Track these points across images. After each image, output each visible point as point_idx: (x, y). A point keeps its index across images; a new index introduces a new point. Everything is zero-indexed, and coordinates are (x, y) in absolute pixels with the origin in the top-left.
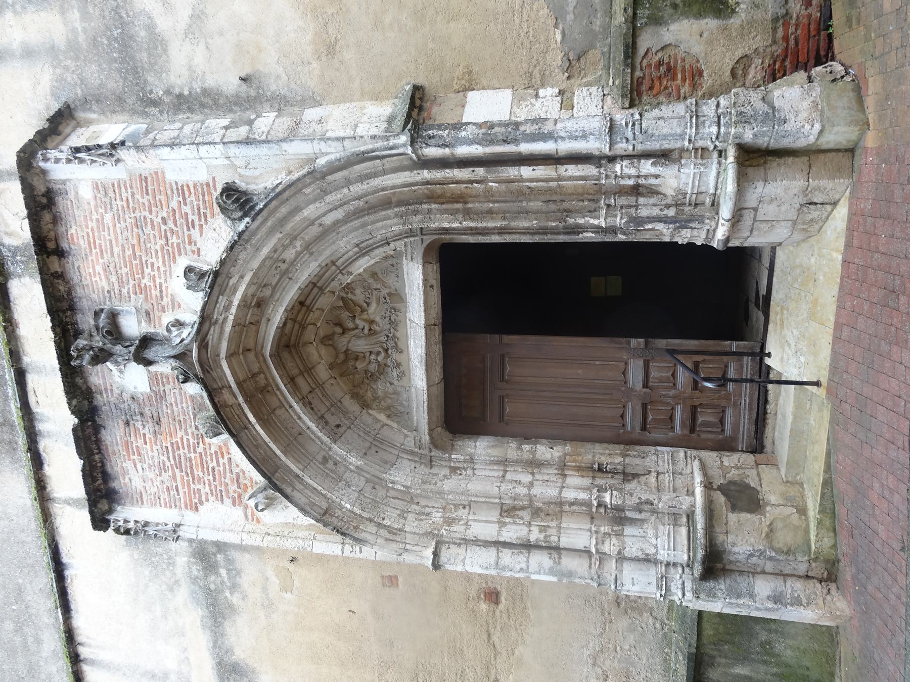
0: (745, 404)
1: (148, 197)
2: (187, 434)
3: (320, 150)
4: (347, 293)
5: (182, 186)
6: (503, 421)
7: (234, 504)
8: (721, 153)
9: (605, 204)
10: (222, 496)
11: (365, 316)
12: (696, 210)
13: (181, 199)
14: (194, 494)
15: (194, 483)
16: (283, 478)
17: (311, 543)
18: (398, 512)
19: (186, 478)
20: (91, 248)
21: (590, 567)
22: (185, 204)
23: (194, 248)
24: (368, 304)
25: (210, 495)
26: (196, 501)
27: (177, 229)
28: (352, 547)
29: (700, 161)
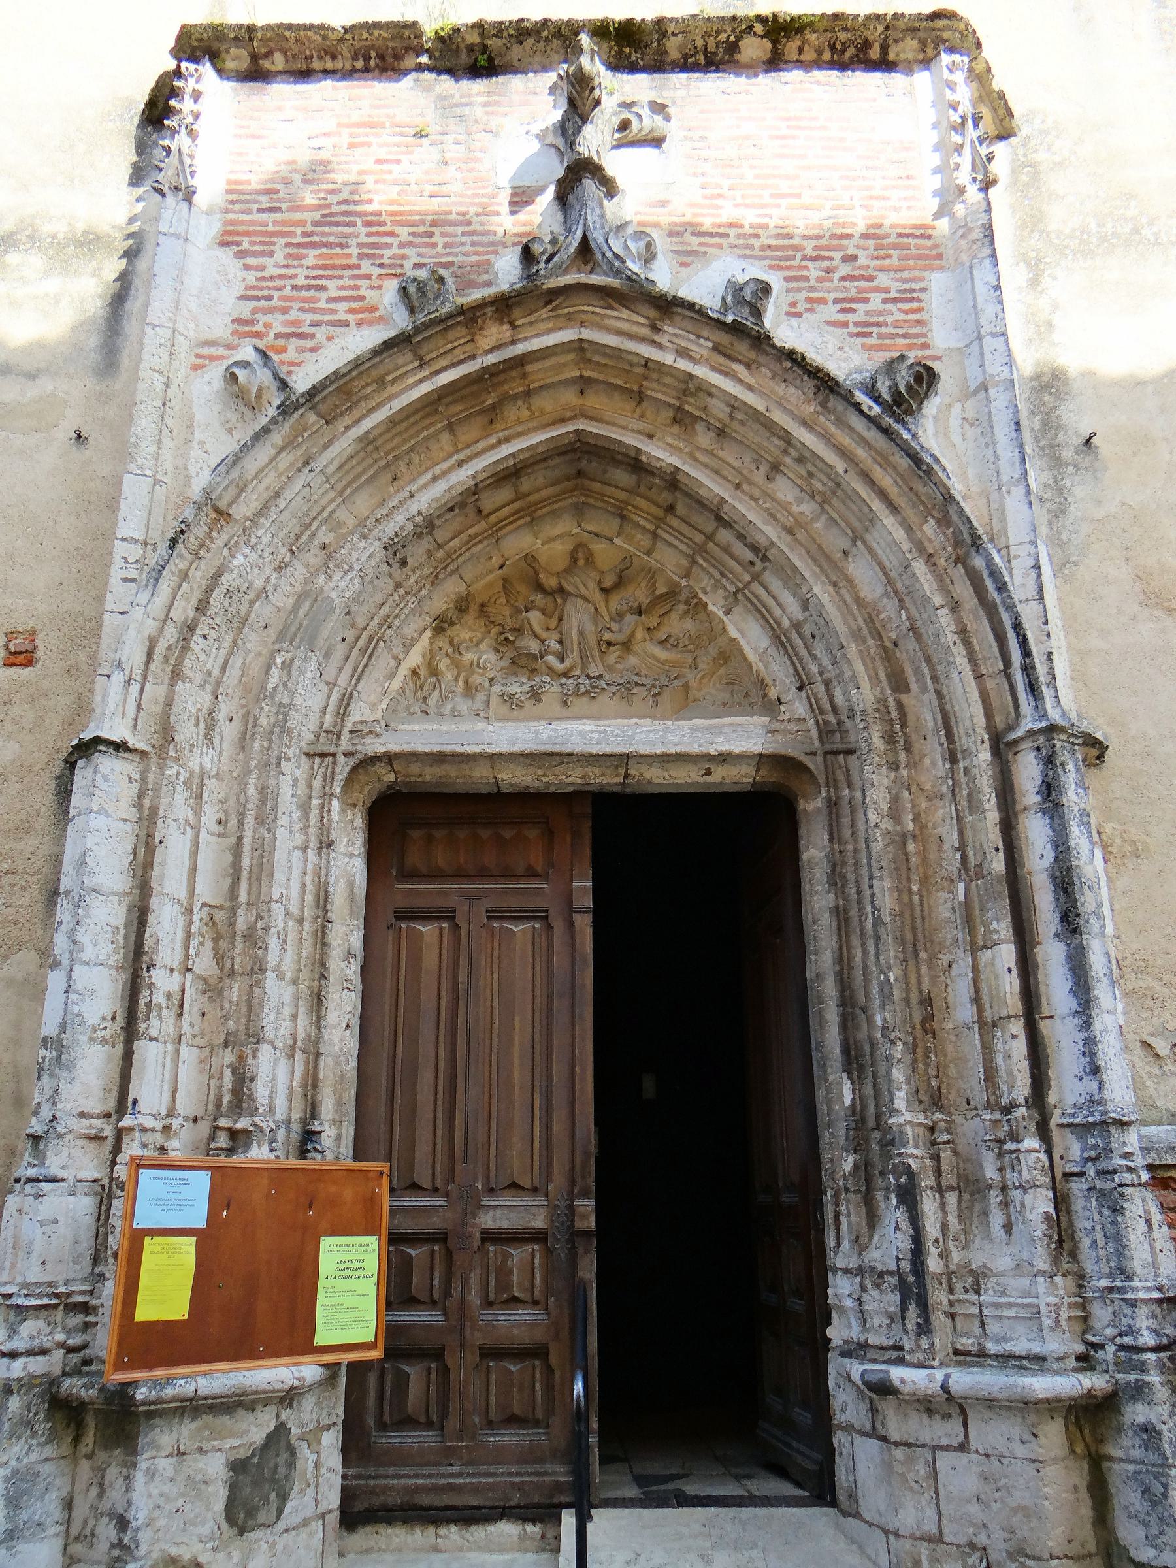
0: (452, 1475)
1: (893, 236)
2: (403, 245)
4: (687, 603)
5: (919, 300)
6: (397, 918)
7: (237, 321)
8: (1085, 1362)
9: (935, 1123)
10: (258, 298)
11: (640, 635)
12: (942, 1317)
13: (893, 295)
14: (262, 243)
15: (287, 245)
16: (305, 430)
17: (148, 472)
18: (216, 672)
19: (299, 231)
20: (789, 119)
21: (82, 1115)
22: (885, 301)
23: (800, 307)
24: (662, 643)
25: (259, 274)
26: (246, 245)
27: (836, 281)
28: (137, 561)
29: (1064, 1315)
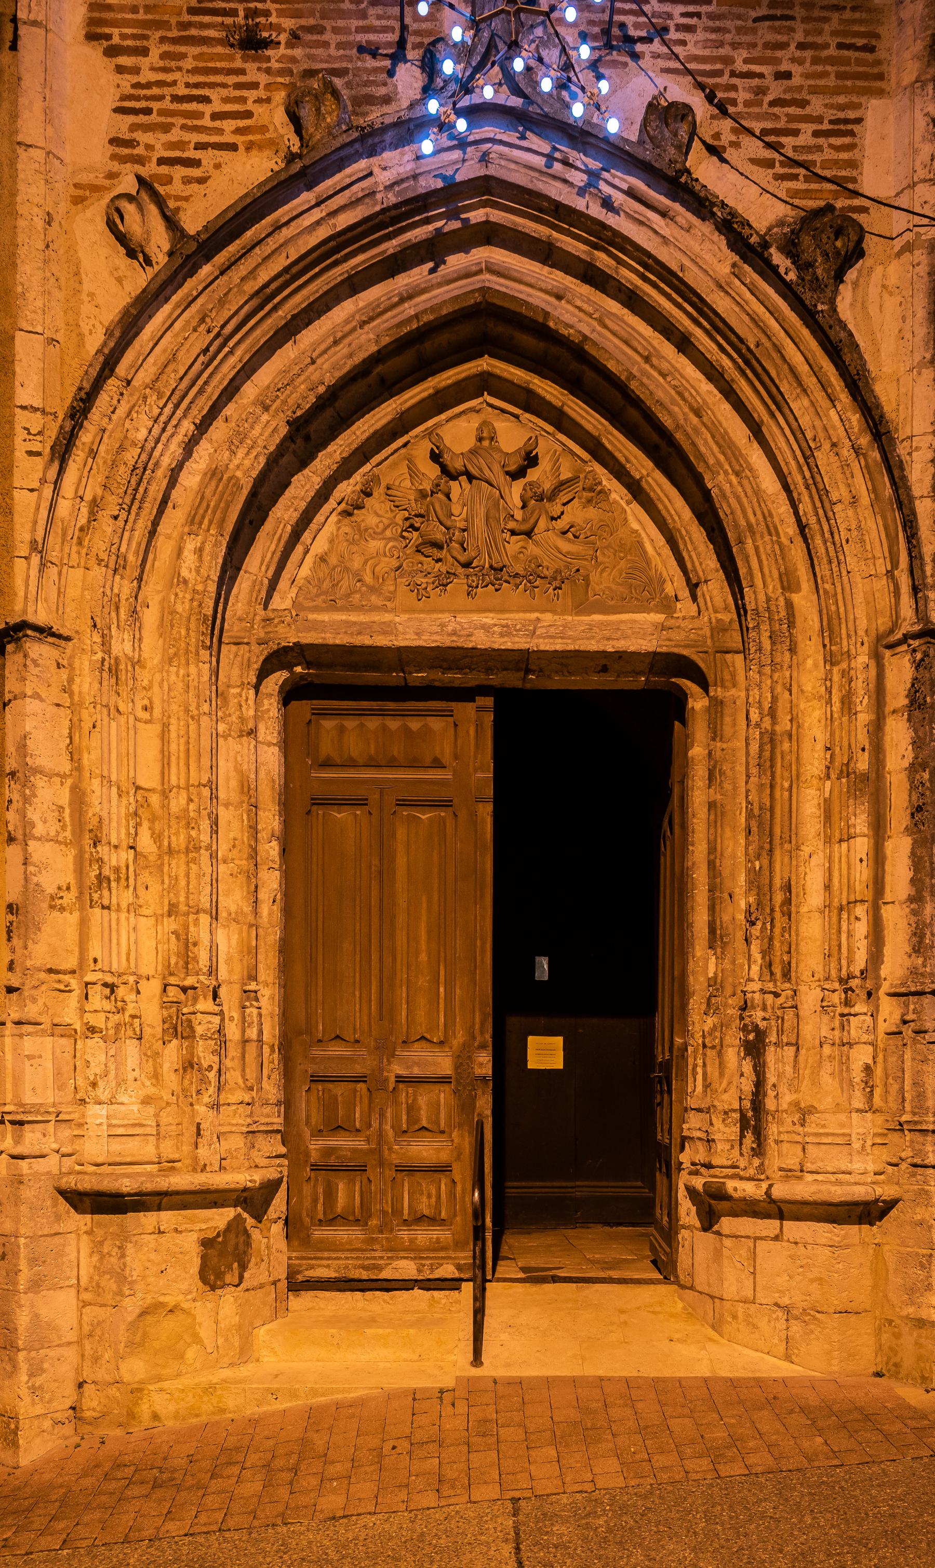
0: (375, 1258)
3: (917, 449)
7: (115, 141)
13: (826, 126)
15: (163, 40)
22: (816, 134)
25: (135, 79)
26: (116, 40)
27: (765, 106)
